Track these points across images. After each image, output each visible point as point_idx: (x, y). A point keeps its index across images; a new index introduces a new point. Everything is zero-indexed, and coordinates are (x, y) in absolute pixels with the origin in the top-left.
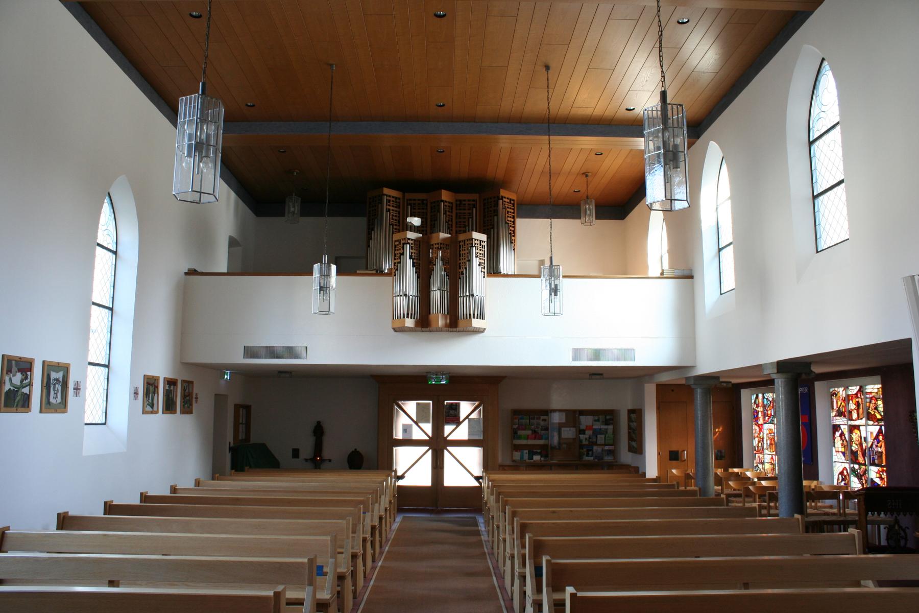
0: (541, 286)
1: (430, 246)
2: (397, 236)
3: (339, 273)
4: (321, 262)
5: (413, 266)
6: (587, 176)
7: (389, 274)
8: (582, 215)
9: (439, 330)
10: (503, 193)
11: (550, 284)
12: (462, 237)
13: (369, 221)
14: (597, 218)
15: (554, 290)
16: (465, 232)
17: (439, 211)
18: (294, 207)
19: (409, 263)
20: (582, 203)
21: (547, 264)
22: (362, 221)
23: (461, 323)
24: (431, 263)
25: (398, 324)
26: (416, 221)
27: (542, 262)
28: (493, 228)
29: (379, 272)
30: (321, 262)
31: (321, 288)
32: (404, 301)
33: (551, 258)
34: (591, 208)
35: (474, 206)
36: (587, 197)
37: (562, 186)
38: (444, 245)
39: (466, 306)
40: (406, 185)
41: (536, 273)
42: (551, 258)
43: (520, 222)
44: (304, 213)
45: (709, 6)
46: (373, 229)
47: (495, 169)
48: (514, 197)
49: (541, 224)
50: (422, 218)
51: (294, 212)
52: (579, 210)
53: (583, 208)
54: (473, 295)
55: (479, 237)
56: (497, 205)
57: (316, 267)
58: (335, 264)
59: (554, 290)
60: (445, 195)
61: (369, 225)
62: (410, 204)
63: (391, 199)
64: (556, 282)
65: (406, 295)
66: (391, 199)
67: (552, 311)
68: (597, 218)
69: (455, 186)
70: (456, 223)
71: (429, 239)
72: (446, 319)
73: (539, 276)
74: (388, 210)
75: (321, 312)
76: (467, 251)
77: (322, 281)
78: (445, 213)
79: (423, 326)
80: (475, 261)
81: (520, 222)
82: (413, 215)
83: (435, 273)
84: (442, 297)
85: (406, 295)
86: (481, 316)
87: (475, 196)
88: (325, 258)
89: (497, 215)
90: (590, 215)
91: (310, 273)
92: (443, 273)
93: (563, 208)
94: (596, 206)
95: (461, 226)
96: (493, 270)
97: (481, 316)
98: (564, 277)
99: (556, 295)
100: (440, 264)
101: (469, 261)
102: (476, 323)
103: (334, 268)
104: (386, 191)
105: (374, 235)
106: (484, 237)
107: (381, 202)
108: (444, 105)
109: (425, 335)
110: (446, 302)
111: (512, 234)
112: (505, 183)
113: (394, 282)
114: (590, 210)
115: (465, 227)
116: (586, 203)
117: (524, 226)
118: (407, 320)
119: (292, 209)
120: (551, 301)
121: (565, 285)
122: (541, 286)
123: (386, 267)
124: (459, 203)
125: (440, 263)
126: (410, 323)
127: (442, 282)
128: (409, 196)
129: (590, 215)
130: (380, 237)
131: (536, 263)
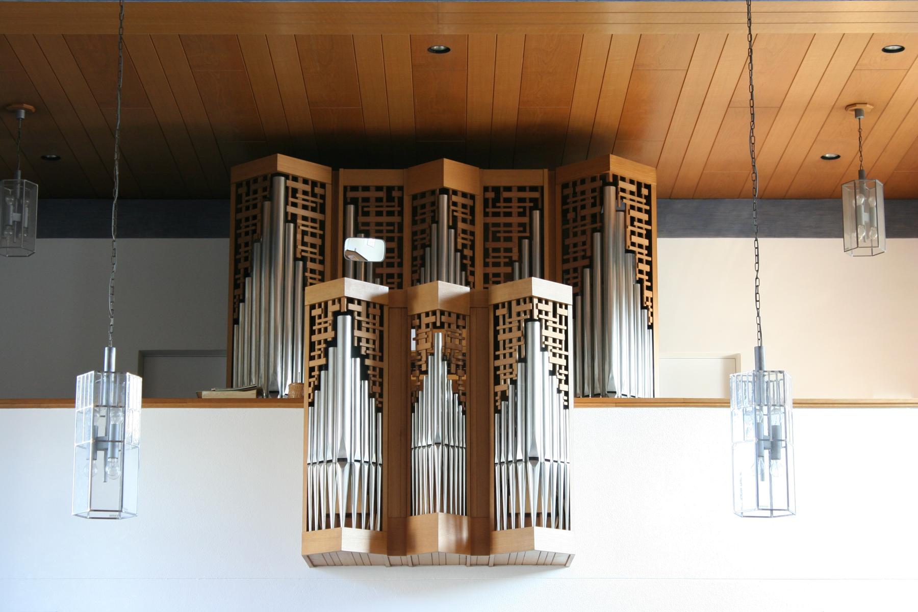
0: (732, 429)
1: (411, 320)
2: (316, 293)
3: (150, 397)
4: (99, 368)
5: (364, 376)
6: (858, 113)
7: (294, 401)
8: (848, 224)
9: (437, 561)
10: (617, 165)
11: (758, 427)
12: (502, 293)
13: (236, 248)
14: (890, 233)
15: (771, 444)
16: (510, 277)
17: (436, 220)
18: (20, 210)
19: (351, 367)
20: (846, 190)
21: (748, 366)
22: (216, 251)
23: (503, 538)
24: (415, 366)
25: (321, 542)
26: (371, 249)
27: (732, 363)
28: (591, 266)
29: (267, 395)
30: (99, 368)
31: (98, 444)
32: (340, 477)
33: (759, 350)
34: (872, 205)
35: (537, 204)
36: (861, 174)
37: (790, 145)
38: (450, 317)
39: (519, 489)
40: (339, 147)
41: (716, 393)
42: (759, 350)
43: (664, 246)
44: (49, 227)
45: (847, 32)
46: (248, 273)
47: (593, 99)
48: (648, 176)
49: (731, 251)
50: (388, 240)
51: (19, 224)
52: (839, 211)
53: (848, 205)
54: (535, 459)
55: (551, 291)
56: (600, 200)
57: (84, 382)
58: (140, 373)
59: (771, 444)
60: (454, 175)
61: (236, 262)
62: (354, 201)
63: (300, 186)
64: (776, 420)
65: (342, 461)
66: (300, 186)
67: (765, 502)
68: (890, 233)
69: (484, 148)
70: (486, 254)
71: (408, 301)
72: (459, 528)
73: (724, 403)
74: (292, 219)
75: (98, 513)
76: (516, 334)
77: (101, 424)
78: (453, 226)
79: (391, 551)
80: (541, 362)
81: (664, 246)
82: (362, 231)
83: (425, 397)
84: (446, 466)
85: (342, 461)
86: (560, 518)
87: (538, 177)
88: (111, 357)
89: (602, 230)
90: (870, 224)
91: (67, 399)
92: (449, 395)
93: (799, 205)
94: (888, 199)
95: (496, 259)
96: (592, 384)
97: (560, 518)
98: (798, 404)
99: (774, 456)
100: (438, 370)
101: (523, 360)
102: (545, 539)
103: (135, 383)
104: (285, 163)
105: (252, 289)
106: (563, 293)
107: (270, 195)
108: (447, 50)
109: (398, 576)
110: (459, 477)
111: (646, 282)
112: (623, 140)
113: (310, 425)
114: (870, 210)
115: (510, 263)
116: (858, 190)
117: (675, 255)
118: (345, 530)
119: (14, 216)
120: (759, 475)
121: (801, 427)
122: (727, 433)
123: (287, 379)
124: (495, 197)
125: (441, 368)
126: (355, 540)
127: (448, 422)
128: (349, 177)
129: (870, 224)
130: (272, 295)
131: (716, 367)
